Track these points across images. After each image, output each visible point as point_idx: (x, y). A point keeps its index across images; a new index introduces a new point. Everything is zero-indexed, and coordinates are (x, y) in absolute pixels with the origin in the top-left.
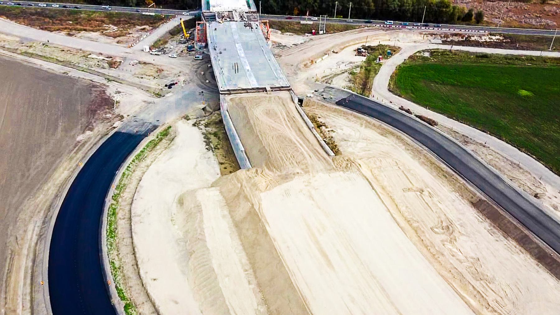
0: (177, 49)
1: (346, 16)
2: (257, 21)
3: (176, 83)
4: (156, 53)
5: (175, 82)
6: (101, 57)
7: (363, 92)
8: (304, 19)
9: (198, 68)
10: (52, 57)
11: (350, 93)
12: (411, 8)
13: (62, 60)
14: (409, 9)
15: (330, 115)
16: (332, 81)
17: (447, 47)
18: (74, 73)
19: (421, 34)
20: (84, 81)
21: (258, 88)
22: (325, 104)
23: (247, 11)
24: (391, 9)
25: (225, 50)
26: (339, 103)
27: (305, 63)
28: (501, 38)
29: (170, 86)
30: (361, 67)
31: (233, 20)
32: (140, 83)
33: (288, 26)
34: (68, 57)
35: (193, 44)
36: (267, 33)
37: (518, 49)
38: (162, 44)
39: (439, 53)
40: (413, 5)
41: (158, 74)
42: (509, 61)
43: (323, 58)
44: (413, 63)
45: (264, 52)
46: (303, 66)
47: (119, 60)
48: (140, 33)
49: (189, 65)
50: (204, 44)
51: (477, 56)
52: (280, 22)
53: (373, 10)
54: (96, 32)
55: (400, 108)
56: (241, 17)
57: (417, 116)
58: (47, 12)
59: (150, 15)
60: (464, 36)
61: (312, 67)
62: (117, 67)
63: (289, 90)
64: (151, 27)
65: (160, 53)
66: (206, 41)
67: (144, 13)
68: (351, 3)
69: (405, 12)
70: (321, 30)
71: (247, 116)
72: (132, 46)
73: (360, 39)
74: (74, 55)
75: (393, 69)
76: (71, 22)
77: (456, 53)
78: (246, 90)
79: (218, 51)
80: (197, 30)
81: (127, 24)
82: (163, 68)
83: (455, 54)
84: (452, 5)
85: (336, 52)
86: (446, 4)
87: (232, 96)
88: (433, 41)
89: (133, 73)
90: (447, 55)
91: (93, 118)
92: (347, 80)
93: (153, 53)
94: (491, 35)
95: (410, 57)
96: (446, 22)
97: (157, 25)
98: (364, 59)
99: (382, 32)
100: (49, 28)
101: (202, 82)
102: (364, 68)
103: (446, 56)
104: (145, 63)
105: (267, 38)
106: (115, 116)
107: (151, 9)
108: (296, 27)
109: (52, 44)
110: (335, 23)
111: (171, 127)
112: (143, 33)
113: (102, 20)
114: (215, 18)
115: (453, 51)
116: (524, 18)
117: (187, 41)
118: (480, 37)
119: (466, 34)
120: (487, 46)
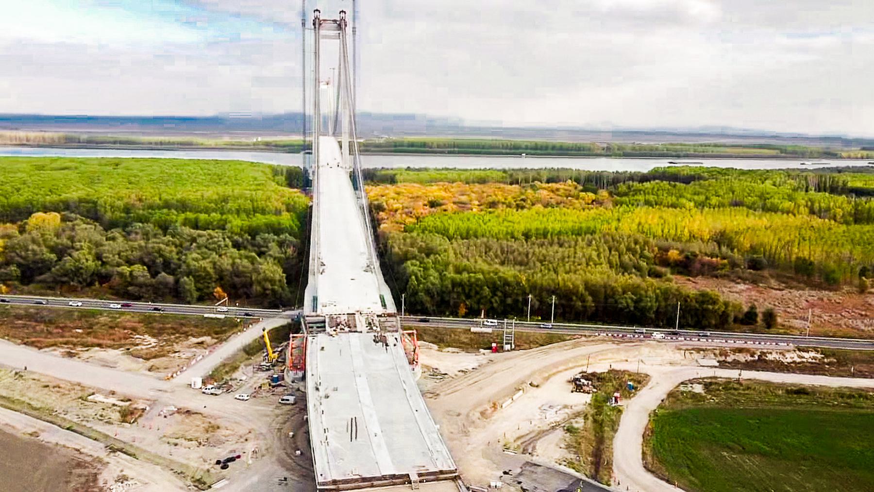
1: (546, 318)
2: (397, 331)
3: (239, 457)
4: (213, 391)
5: (235, 455)
8: (477, 324)
9: (285, 423)
10: (22, 399)
11: (572, 477)
12: (655, 305)
13: (39, 406)
14: (652, 306)
18: (52, 436)
20: (64, 451)
21: (393, 477)
23: (380, 313)
24: (620, 306)
25: (336, 389)
27: (480, 409)
29: (224, 464)
30: (586, 417)
33: (450, 336)
34: (51, 400)
35: (283, 371)
36: (414, 351)
37: (853, 376)
38: (227, 373)
39: (720, 385)
41: (208, 435)
42: (849, 401)
43: (514, 398)
44: (678, 407)
45: (408, 394)
47: (141, 406)
49: (268, 416)
50: (300, 374)
51: (788, 392)
53: (591, 307)
54: (117, 349)
56: (370, 324)
58: (45, 313)
60: (754, 353)
63: (455, 479)
65: (219, 392)
66: (303, 368)
67: (206, 315)
68: (554, 297)
69: (643, 311)
73: (575, 358)
74: (64, 395)
76: (80, 331)
77: (750, 386)
79: (322, 393)
80: (290, 348)
83: (748, 388)
89: (161, 433)
90: (735, 389)
92: (563, 446)
93: (207, 391)
94: (799, 350)
95: (671, 395)
96: (717, 327)
97: (224, 336)
98: (588, 398)
99: (611, 346)
100: (39, 342)
101: (288, 456)
103: (733, 391)
104: (188, 412)
105: (412, 362)
108: (464, 338)
109: (32, 373)
112: (198, 351)
114: (325, 327)
115: (744, 383)
116: (841, 319)
117: (274, 366)
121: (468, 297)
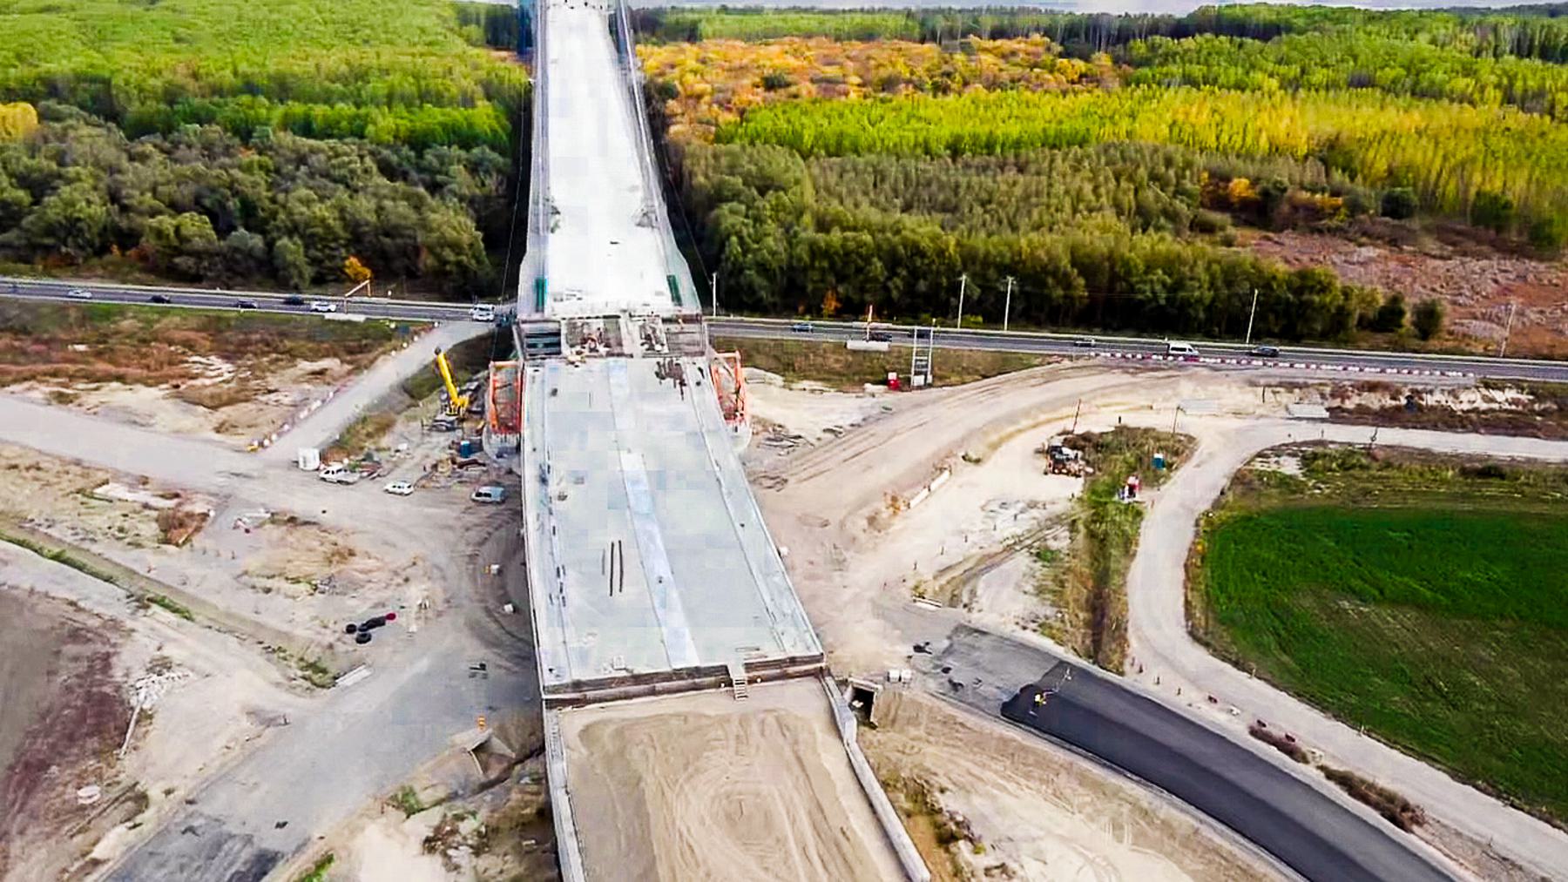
0: (418, 454)
1: (993, 319)
3: (392, 617)
4: (341, 476)
6: (143, 496)
7: (1097, 643)
11: (1045, 655)
12: (1209, 295)
15: (987, 775)
16: (973, 593)
17: (1359, 435)
19: (1253, 384)
20: (43, 607)
21: (696, 672)
22: (961, 716)
23: (666, 315)
24: (1140, 297)
26: (1017, 710)
27: (867, 512)
28: (1524, 397)
29: (363, 632)
31: (617, 350)
32: (254, 617)
36: (737, 392)
38: (369, 435)
40: (1212, 285)
46: (864, 523)
47: (199, 508)
48: (307, 386)
49: (450, 528)
51: (1464, 472)
52: (779, 344)
53: (1081, 297)
54: (156, 384)
55: (1253, 733)
56: (648, 338)
57: (1330, 775)
59: (349, 322)
60: (1399, 392)
61: (898, 524)
62: (184, 543)
63: (819, 674)
64: (349, 363)
65: (355, 477)
70: (917, 373)
71: (646, 841)
72: (261, 444)
73: (1053, 405)
74: (48, 484)
75: (1184, 536)
76: (81, 348)
77: (1393, 459)
78: (646, 684)
81: (265, 354)
82: (356, 543)
84: (1338, 284)
85: (974, 457)
86: (1320, 282)
87: (590, 714)
88: (1298, 411)
90: (1362, 467)
91: (23, 804)
93: (329, 476)
94: (1487, 386)
98: (1076, 486)
101: (488, 612)
102: (1081, 527)
104: (292, 520)
106: (115, 791)
107: (357, 299)
108: (832, 362)
110: (963, 348)
111: (329, 859)
113: (188, 340)
114: (559, 344)
115: (1380, 454)
117: (462, 420)
118: (1453, 393)
119: (1405, 384)
120: (1485, 426)
121: (842, 278)
